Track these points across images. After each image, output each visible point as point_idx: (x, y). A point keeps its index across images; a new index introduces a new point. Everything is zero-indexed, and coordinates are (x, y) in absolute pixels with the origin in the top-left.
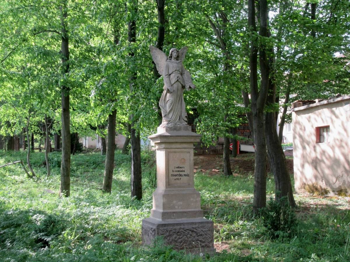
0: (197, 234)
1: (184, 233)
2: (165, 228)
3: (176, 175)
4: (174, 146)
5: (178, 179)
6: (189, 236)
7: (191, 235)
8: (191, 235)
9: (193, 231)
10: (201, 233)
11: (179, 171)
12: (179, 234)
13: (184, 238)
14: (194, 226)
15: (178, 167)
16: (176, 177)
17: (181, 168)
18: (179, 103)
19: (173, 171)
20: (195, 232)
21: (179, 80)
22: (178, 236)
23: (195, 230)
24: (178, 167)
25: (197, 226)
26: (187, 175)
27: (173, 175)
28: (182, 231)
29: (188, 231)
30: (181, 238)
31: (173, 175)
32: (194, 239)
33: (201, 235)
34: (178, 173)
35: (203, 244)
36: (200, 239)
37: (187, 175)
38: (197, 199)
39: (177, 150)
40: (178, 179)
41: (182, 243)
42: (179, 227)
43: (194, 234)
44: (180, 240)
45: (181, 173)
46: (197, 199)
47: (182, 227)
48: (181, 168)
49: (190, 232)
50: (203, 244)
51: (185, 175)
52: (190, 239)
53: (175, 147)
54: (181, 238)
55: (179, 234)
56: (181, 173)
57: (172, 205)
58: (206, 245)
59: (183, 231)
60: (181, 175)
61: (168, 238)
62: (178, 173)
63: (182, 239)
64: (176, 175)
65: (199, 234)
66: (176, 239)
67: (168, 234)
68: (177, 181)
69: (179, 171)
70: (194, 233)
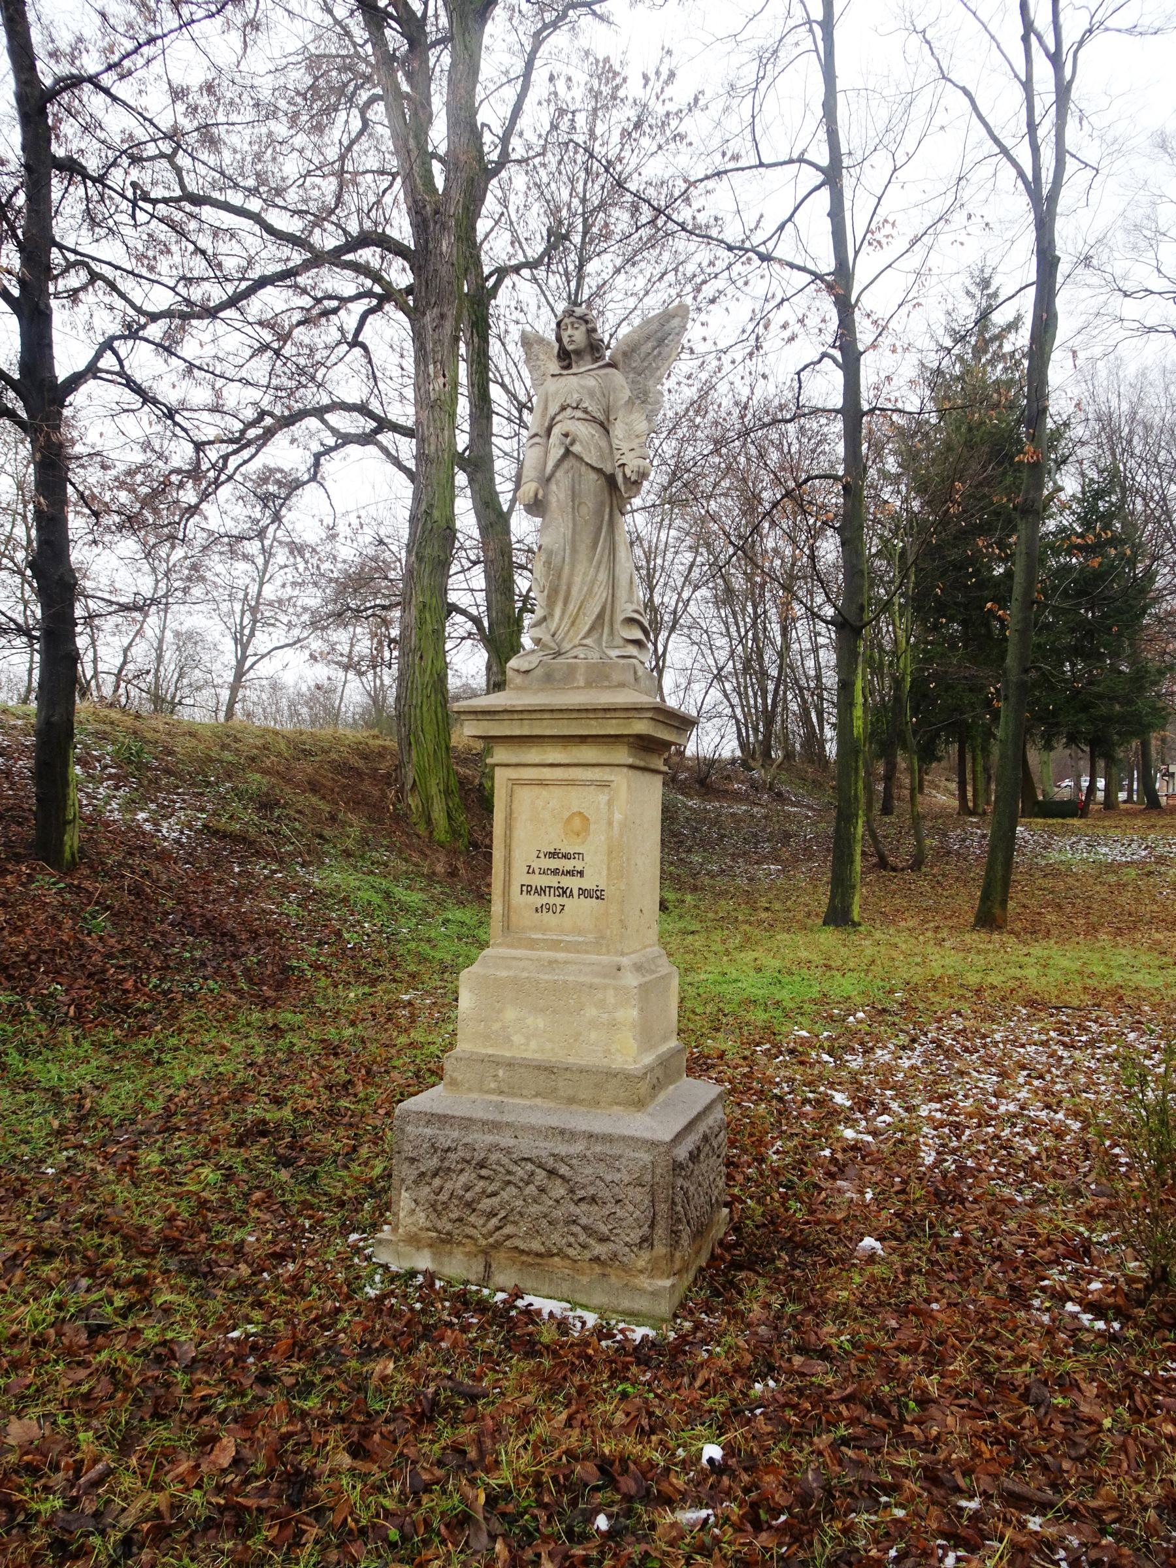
0: (572, 1191)
1: (509, 1173)
2: (428, 1131)
3: (541, 891)
4: (533, 755)
5: (549, 908)
6: (531, 1189)
7: (542, 1190)
8: (542, 1190)
9: (552, 1173)
10: (591, 1191)
11: (555, 872)
12: (484, 1172)
13: (504, 1195)
14: (562, 1149)
15: (553, 855)
16: (544, 900)
17: (565, 856)
18: (591, 560)
19: (530, 871)
20: (562, 1177)
21: (576, 448)
22: (482, 1183)
23: (563, 1170)
24: (553, 855)
25: (578, 1147)
26: (596, 894)
27: (528, 889)
28: (498, 1163)
29: (529, 1167)
30: (494, 1194)
31: (528, 889)
32: (558, 1214)
33: (593, 1200)
34: (552, 881)
35: (600, 1249)
36: (584, 1221)
37: (596, 894)
38: (620, 1015)
39: (547, 773)
40: (549, 908)
41: (494, 1221)
42: (489, 1139)
43: (559, 1190)
44: (486, 1204)
45: (566, 882)
46: (620, 1015)
47: (506, 1141)
48: (565, 856)
49: (541, 1174)
50: (600, 1249)
51: (583, 892)
52: (534, 1209)
53: (537, 761)
54: (494, 1194)
55: (484, 1172)
56: (566, 882)
57: (496, 1026)
58: (614, 1256)
59: (505, 1161)
60: (564, 892)
61: (437, 1182)
62: (552, 881)
63: (495, 1200)
64: (541, 891)
65: (581, 1193)
66: (469, 1196)
67: (434, 1162)
68: (547, 917)
69: (555, 872)
70: (559, 1182)
